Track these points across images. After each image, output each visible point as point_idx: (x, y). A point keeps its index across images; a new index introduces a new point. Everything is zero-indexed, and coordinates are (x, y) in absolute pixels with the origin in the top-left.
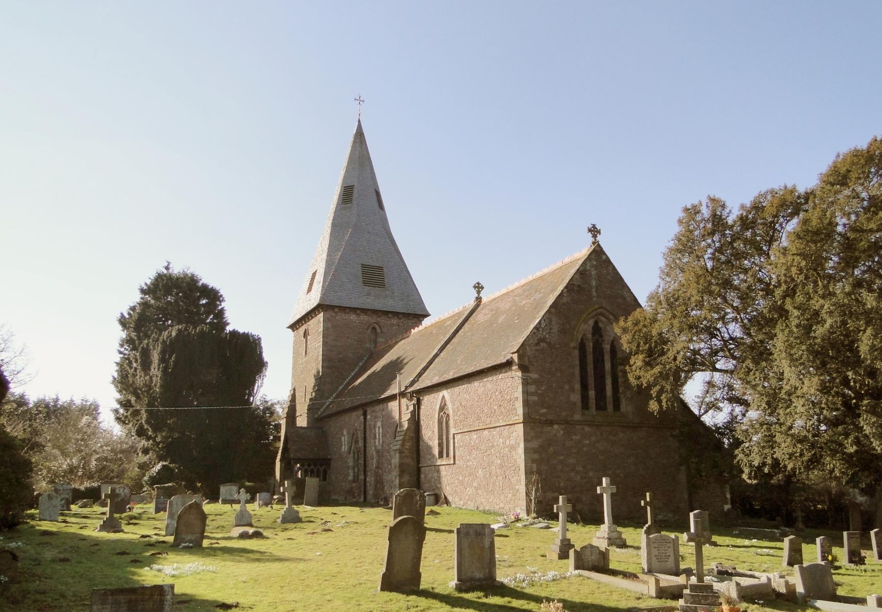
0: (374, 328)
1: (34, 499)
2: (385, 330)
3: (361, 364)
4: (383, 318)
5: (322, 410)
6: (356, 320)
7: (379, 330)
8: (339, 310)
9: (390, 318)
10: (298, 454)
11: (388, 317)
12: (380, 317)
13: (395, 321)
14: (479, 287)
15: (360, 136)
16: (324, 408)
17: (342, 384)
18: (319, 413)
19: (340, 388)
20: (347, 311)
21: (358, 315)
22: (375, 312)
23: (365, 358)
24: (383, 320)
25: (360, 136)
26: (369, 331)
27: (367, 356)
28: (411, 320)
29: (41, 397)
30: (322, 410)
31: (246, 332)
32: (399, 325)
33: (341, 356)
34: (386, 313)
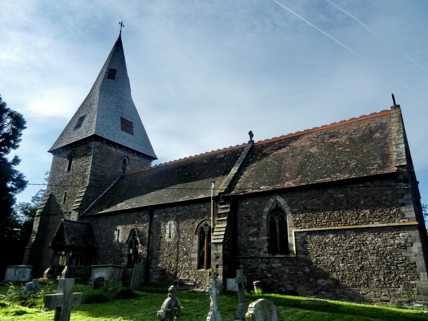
0: (125, 160)
1: (133, 257)
2: (131, 162)
3: (115, 182)
4: (131, 155)
5: (86, 210)
6: (115, 152)
7: (127, 162)
8: (106, 142)
9: (135, 155)
10: (73, 242)
11: (134, 155)
12: (129, 153)
13: (137, 158)
14: (251, 134)
15: (119, 44)
16: (87, 209)
17: (101, 194)
18: (84, 212)
19: (100, 196)
20: (111, 144)
21: (116, 148)
22: (127, 149)
23: (118, 179)
24: (130, 156)
25: (119, 44)
26: (122, 161)
27: (119, 177)
28: (146, 159)
29: (21, 113)
30: (86, 210)
31: (17, 149)
32: (139, 161)
33: (103, 174)
34: (133, 151)
